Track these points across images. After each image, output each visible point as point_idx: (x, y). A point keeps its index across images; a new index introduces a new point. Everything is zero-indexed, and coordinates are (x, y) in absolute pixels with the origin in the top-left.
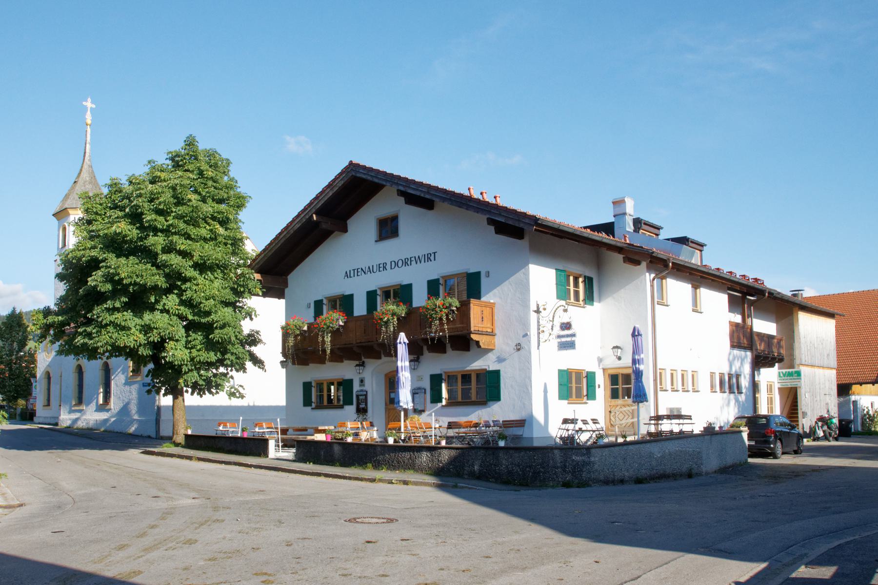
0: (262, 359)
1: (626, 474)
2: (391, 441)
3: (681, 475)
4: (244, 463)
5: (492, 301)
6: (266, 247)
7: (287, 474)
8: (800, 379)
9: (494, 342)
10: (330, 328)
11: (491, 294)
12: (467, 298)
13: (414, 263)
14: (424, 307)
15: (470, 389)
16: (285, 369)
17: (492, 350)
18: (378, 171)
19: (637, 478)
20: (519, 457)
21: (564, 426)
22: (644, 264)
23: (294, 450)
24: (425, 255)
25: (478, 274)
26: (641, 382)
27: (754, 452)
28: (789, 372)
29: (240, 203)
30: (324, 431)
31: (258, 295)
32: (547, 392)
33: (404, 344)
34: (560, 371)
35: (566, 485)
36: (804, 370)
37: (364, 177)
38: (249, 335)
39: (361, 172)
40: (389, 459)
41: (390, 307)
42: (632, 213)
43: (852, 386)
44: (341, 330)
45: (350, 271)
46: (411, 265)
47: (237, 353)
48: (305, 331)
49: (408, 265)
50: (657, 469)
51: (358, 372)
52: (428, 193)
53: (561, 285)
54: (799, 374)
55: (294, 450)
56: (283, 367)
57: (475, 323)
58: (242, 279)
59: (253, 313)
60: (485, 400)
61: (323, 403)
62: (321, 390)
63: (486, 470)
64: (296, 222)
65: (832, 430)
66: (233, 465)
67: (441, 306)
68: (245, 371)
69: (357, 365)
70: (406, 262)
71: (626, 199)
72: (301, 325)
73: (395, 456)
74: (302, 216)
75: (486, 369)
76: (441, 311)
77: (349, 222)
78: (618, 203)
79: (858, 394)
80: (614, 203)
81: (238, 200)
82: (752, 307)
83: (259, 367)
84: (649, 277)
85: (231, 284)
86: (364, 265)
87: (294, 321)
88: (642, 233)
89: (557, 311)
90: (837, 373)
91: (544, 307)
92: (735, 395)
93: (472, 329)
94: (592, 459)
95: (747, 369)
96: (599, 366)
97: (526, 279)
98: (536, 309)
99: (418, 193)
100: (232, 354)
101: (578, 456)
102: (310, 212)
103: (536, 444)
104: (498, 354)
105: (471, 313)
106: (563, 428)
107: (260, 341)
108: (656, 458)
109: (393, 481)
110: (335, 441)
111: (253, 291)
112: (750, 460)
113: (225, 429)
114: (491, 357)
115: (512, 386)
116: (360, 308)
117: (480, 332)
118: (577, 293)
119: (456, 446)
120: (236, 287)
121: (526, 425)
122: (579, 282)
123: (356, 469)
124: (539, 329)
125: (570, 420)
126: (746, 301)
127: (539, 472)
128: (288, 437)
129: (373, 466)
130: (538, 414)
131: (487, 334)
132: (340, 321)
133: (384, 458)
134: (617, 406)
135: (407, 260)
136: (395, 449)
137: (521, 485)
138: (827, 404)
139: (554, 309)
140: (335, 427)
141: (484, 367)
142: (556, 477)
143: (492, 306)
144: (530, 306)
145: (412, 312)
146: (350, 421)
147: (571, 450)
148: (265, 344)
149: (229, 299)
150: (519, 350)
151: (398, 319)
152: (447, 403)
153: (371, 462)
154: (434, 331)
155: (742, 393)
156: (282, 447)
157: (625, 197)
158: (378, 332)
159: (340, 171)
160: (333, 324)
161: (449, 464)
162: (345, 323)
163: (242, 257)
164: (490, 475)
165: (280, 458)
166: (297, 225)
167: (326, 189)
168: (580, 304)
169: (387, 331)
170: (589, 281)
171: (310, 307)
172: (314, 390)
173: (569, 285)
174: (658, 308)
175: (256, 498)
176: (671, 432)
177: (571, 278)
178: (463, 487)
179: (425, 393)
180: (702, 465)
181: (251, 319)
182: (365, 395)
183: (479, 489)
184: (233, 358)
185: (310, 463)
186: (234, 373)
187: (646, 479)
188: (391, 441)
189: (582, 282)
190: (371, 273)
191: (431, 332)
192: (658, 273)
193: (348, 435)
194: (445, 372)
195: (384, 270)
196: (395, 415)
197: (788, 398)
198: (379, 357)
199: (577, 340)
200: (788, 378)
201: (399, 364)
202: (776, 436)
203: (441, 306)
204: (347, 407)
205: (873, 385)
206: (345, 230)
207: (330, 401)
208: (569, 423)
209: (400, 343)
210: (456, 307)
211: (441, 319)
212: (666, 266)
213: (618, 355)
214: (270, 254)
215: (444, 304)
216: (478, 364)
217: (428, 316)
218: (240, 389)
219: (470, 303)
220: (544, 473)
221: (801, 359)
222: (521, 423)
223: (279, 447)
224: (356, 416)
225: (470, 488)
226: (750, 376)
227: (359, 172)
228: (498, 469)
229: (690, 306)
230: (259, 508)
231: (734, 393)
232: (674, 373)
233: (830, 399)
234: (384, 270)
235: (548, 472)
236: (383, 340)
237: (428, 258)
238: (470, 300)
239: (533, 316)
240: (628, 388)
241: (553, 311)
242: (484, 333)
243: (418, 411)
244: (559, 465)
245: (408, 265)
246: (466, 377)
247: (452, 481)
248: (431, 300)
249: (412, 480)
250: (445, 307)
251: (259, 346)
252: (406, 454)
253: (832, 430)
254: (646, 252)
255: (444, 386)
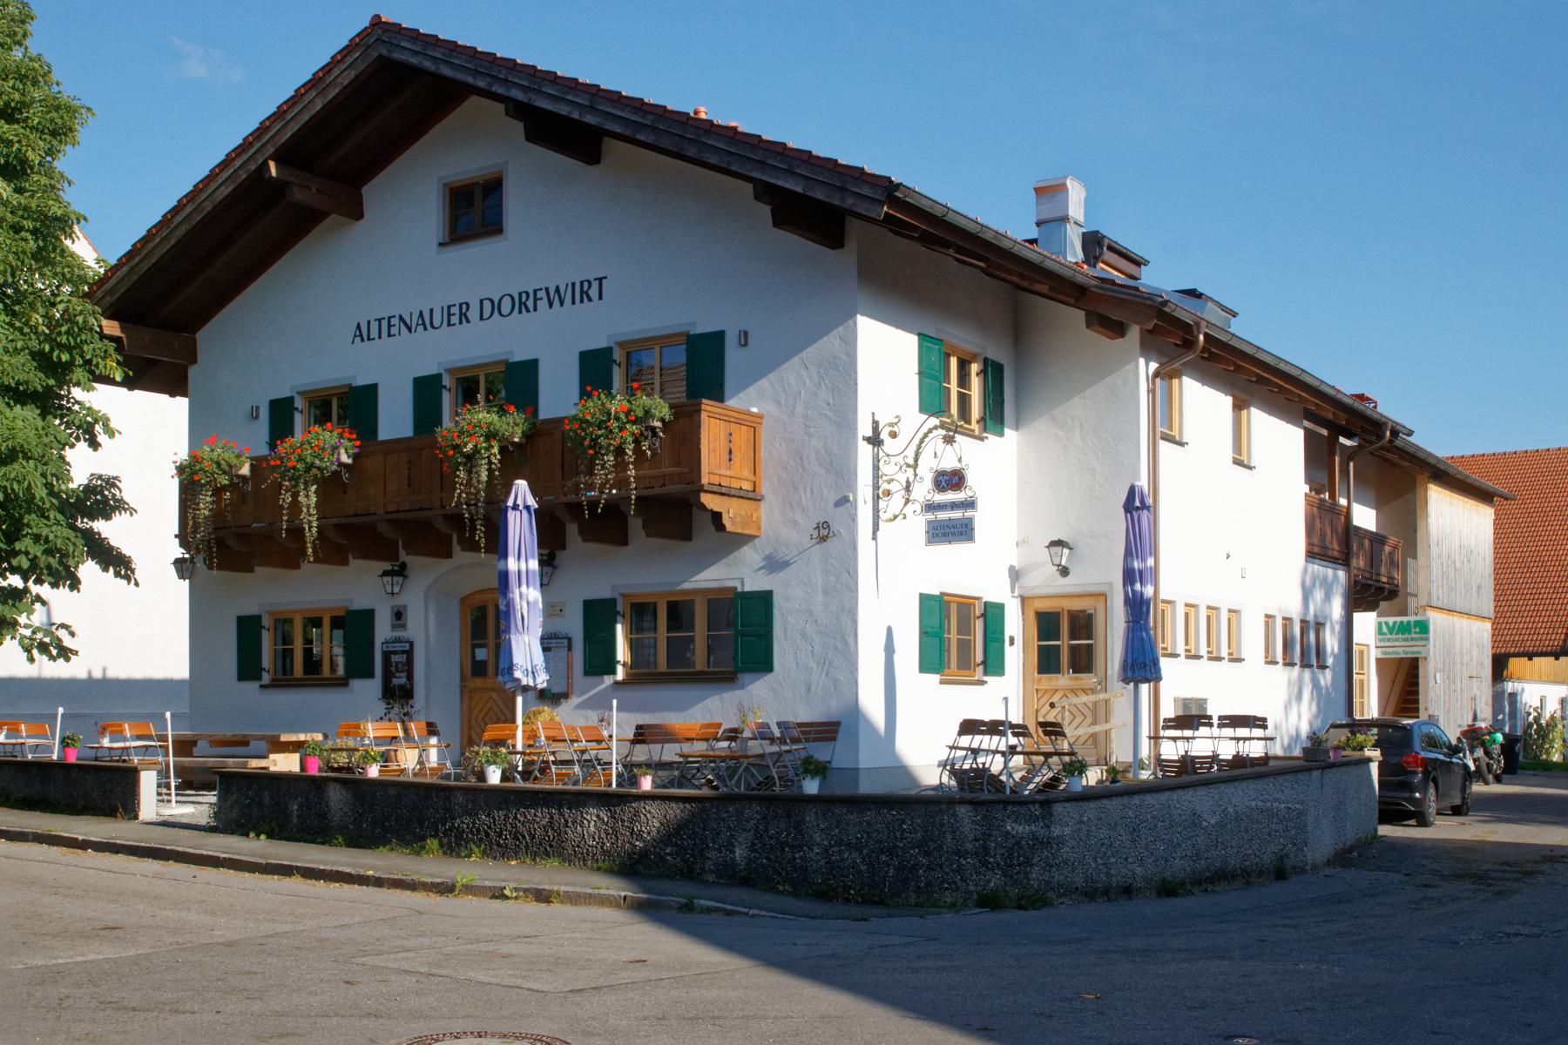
0: (126, 551)
1: (1139, 871)
2: (494, 776)
3: (1260, 874)
4: (66, 835)
5: (755, 410)
6: (134, 245)
7: (191, 869)
8: (1427, 639)
9: (759, 518)
10: (314, 470)
11: (751, 390)
12: (689, 397)
13: (542, 304)
14: (574, 418)
15: (692, 639)
16: (187, 581)
17: (750, 538)
18: (452, 47)
19: (1164, 880)
20: (861, 823)
21: (965, 741)
22: (1134, 333)
23: (212, 797)
24: (573, 284)
25: (719, 337)
26: (1146, 628)
27: (1391, 814)
28: (1402, 622)
29: (59, 122)
30: (296, 746)
31: (108, 380)
32: (894, 652)
33: (525, 513)
34: (924, 598)
35: (989, 902)
36: (1436, 619)
37: (414, 60)
38: (89, 490)
39: (405, 48)
40: (490, 828)
41: (481, 416)
42: (1081, 219)
43: (1508, 661)
44: (345, 476)
45: (369, 322)
46: (535, 309)
47: (51, 537)
48: (243, 477)
49: (528, 311)
50: (1207, 858)
51: (389, 590)
52: (592, 109)
53: (931, 377)
54: (1423, 627)
55: (212, 797)
56: (182, 576)
57: (712, 466)
58: (64, 329)
59: (98, 428)
60: (732, 669)
61: (292, 673)
62: (287, 639)
63: (768, 859)
64: (220, 181)
65: (1492, 758)
66: (33, 841)
67: (622, 416)
68: (75, 584)
69: (386, 573)
70: (523, 303)
71: (1069, 183)
72: (234, 461)
73: (506, 816)
74: (238, 163)
75: (736, 588)
76: (621, 429)
77: (365, 190)
78: (1050, 192)
79: (1518, 679)
80: (1038, 191)
81: (54, 114)
82: (1351, 464)
83: (117, 574)
84: (1146, 368)
85: (34, 344)
86: (409, 307)
87: (212, 450)
88: (1102, 269)
89: (927, 440)
90: (1494, 630)
91: (891, 429)
92: (1313, 673)
93: (705, 481)
94: (1056, 831)
95: (1337, 608)
96: (1013, 591)
97: (848, 355)
98: (869, 433)
99: (563, 110)
100: (37, 538)
101: (1020, 824)
102: (259, 155)
103: (866, 787)
104: (768, 551)
105: (702, 436)
106: (993, 747)
107: (120, 506)
108: (1205, 829)
109: (507, 892)
110: (330, 774)
111: (97, 365)
112: (1385, 830)
113: (13, 741)
114: (749, 555)
115: (804, 635)
116: (395, 420)
117: (724, 490)
118: (964, 400)
119: (565, 787)
120: (47, 348)
121: (840, 736)
122: (969, 374)
123: (393, 854)
124: (876, 487)
125: (983, 723)
126: (1338, 448)
127: (915, 867)
128: (197, 762)
129: (441, 845)
130: (871, 702)
131: (741, 495)
132: (342, 451)
133: (474, 823)
134: (1057, 690)
135: (524, 296)
136: (504, 798)
137: (868, 901)
138: (1474, 699)
139: (920, 435)
140: (326, 737)
141: (730, 584)
142: (962, 880)
143: (753, 423)
144: (856, 424)
145: (538, 432)
146: (372, 721)
147: (1001, 806)
148: (132, 511)
149: (27, 382)
150: (823, 539)
151: (502, 450)
152: (627, 674)
153: (436, 836)
154: (600, 486)
155: (1327, 667)
156: (176, 789)
157: (1066, 177)
158: (447, 484)
159: (345, 42)
160: (322, 460)
161: (662, 841)
162: (356, 457)
163: (68, 276)
164: (780, 874)
165: (171, 819)
166: (223, 188)
167: (306, 92)
168: (973, 431)
169: (469, 480)
170: (994, 374)
171: (257, 417)
172: (267, 639)
173: (948, 379)
174: (1164, 447)
175: (92, 957)
176: (1214, 758)
177: (954, 361)
178: (709, 910)
179: (570, 648)
180: (1306, 845)
181: (94, 444)
182: (403, 652)
183: (753, 916)
184: (36, 550)
185: (258, 836)
186: (44, 590)
187: (1184, 884)
188: (494, 776)
189: (977, 374)
190: (426, 329)
191: (591, 487)
192: (1164, 360)
193: (368, 758)
194: (624, 596)
195: (461, 323)
196: (488, 706)
197: (1394, 682)
198: (443, 551)
199: (980, 518)
200: (1400, 636)
201: (512, 564)
202: (1426, 773)
203: (622, 416)
204: (357, 684)
205: (1557, 659)
206: (357, 213)
207: (312, 665)
208: (982, 733)
209: (515, 507)
210: (662, 420)
211: (620, 451)
212: (1189, 344)
213: (1063, 563)
214: (144, 268)
215: (630, 411)
216: (713, 576)
217: (586, 443)
218: (62, 633)
219: (699, 411)
220: (929, 868)
221: (1430, 594)
222: (827, 731)
223: (169, 788)
224: (382, 706)
225: (729, 913)
226: (1341, 626)
227: (398, 46)
228: (801, 858)
229: (1229, 454)
230: (94, 1003)
231: (1310, 666)
232: (1192, 611)
233: (1478, 688)
234: (461, 323)
235: (941, 866)
236: (459, 504)
237: (582, 292)
238: (700, 404)
239: (865, 452)
240: (1088, 645)
241: (916, 441)
242: (733, 492)
243: (549, 697)
244: (969, 846)
245: (528, 311)
246: (679, 613)
247: (676, 892)
248: (595, 399)
249: (563, 888)
250: (633, 418)
251: (119, 519)
252: (539, 814)
253: (1492, 758)
254: (1148, 302)
255: (619, 628)
